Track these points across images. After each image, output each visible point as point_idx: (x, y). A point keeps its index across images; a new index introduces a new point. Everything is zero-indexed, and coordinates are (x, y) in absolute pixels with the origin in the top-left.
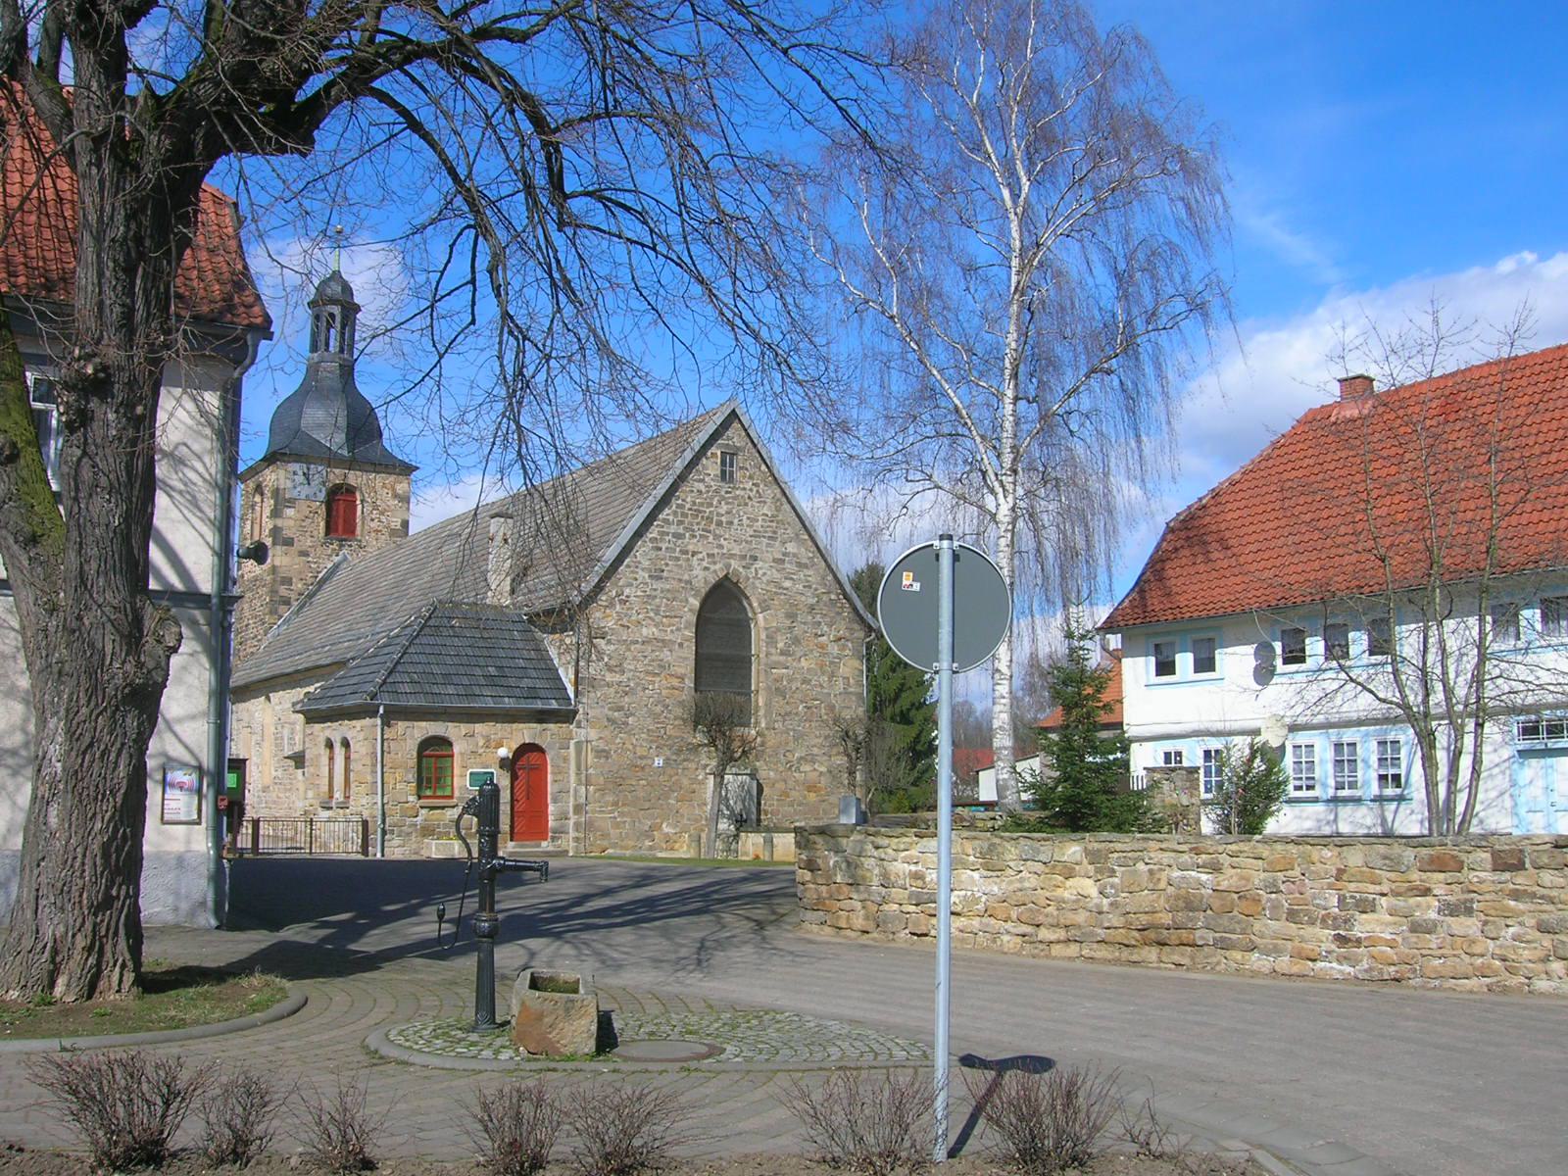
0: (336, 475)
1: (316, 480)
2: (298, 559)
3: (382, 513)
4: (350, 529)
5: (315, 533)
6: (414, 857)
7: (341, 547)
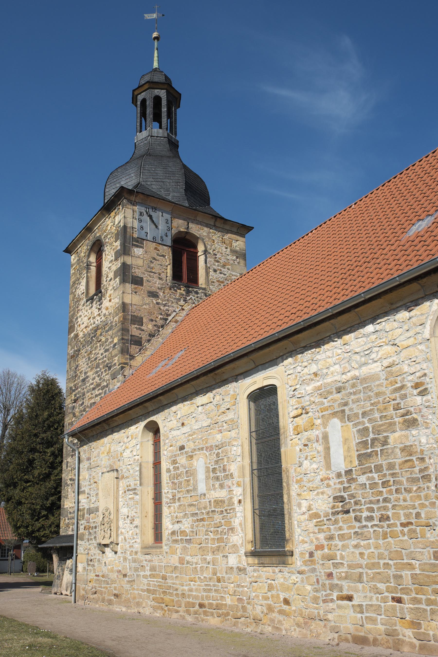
0: (179, 225)
1: (162, 226)
2: (148, 300)
3: (224, 266)
4: (193, 279)
5: (163, 276)
6: (90, 444)
7: (188, 292)
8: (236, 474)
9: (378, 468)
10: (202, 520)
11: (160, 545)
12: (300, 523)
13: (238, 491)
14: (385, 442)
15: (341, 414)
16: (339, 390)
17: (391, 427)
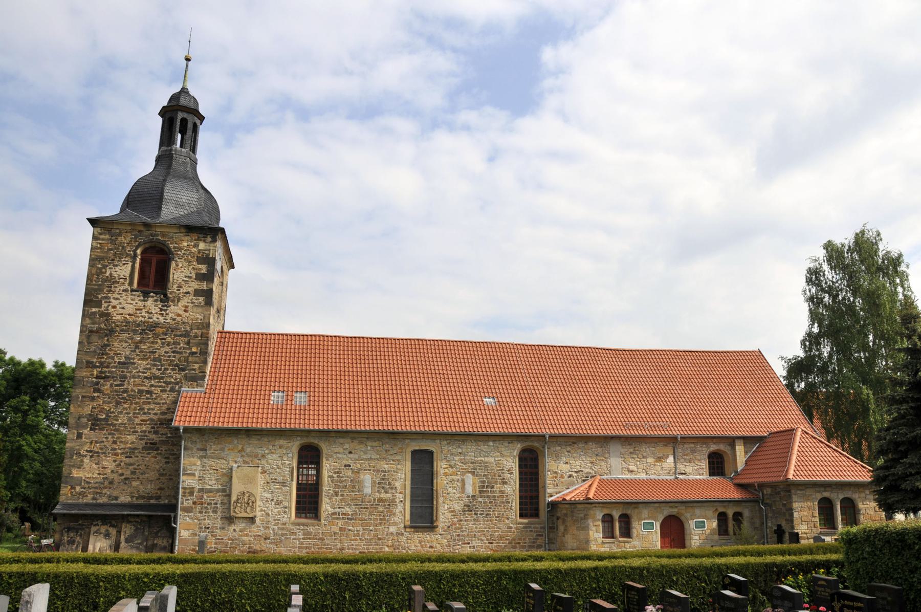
8: (399, 487)
9: (488, 497)
10: (345, 514)
11: (151, 283)
12: (443, 514)
13: (400, 497)
14: (493, 487)
15: (473, 474)
16: (472, 463)
17: (496, 482)
